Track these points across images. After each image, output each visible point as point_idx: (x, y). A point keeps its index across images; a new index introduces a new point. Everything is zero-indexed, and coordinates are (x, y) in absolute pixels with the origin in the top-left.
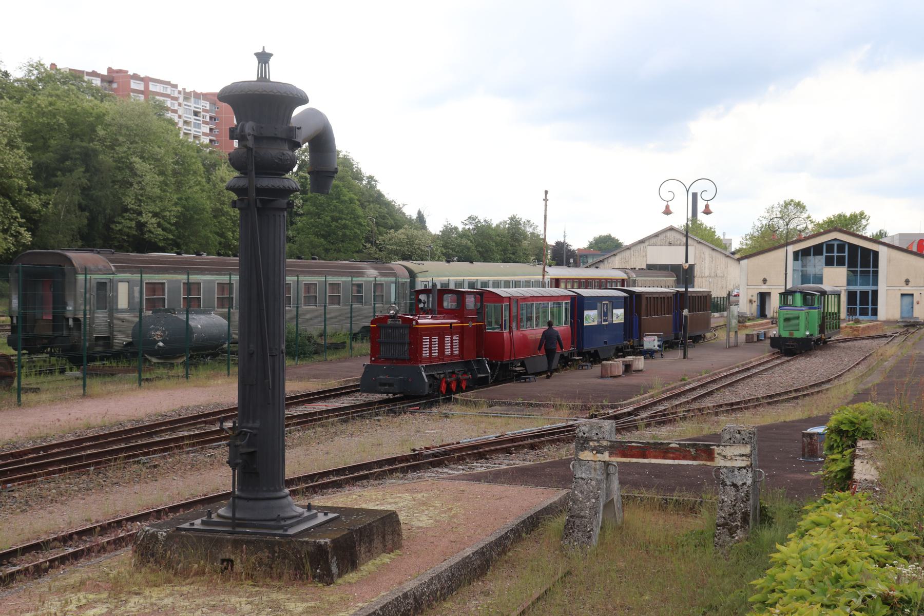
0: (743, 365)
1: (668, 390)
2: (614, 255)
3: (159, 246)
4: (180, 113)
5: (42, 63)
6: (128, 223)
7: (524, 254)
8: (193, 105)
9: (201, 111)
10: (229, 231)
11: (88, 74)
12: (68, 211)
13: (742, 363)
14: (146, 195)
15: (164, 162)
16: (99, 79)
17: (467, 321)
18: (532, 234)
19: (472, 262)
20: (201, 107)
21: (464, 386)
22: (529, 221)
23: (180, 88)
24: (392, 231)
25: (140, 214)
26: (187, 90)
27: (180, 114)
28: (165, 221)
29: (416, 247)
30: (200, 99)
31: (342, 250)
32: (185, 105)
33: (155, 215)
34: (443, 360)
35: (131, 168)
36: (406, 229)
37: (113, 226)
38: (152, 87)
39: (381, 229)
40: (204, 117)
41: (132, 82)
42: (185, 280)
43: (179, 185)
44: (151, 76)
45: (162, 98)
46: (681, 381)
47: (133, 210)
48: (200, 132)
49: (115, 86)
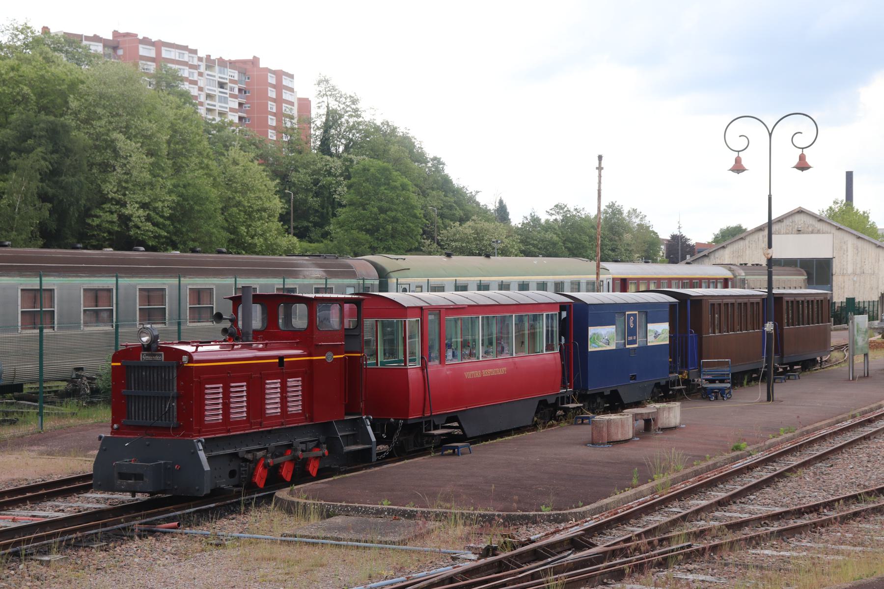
0: (864, 413)
1: (696, 473)
2: (723, 247)
4: (201, 83)
5: (29, 25)
6: (108, 217)
7: (626, 250)
8: (217, 74)
9: (227, 81)
10: (242, 225)
11: (88, 38)
12: (24, 201)
13: (860, 410)
14: (133, 181)
15: (155, 140)
16: (101, 45)
17: (323, 351)
18: (640, 226)
19: (488, 256)
20: (228, 77)
21: (313, 469)
22: (635, 210)
23: (200, 54)
24: (457, 224)
25: (124, 205)
26: (212, 58)
27: (202, 86)
28: (157, 214)
30: (227, 67)
32: (208, 75)
33: (144, 206)
34: (260, 424)
35: (111, 145)
37: (89, 221)
38: (166, 53)
39: (447, 221)
40: (232, 89)
41: (141, 46)
43: (178, 170)
44: (163, 40)
45: (175, 67)
46: (733, 450)
47: (116, 200)
48: (227, 108)
49: (120, 52)
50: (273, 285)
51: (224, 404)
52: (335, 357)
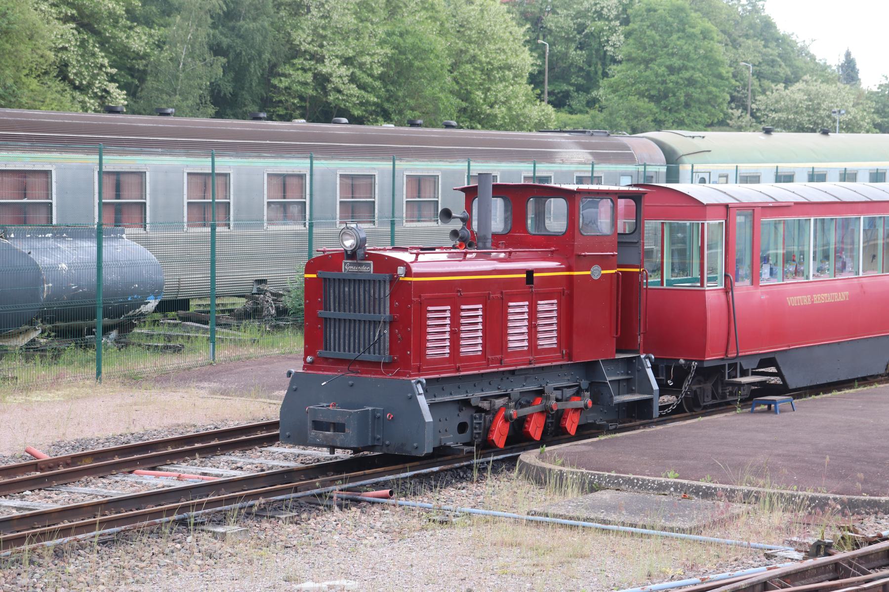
3: (353, 115)
6: (299, 76)
19: (825, 132)
21: (571, 425)
25: (321, 60)
29: (823, 113)
31: (686, 121)
33: (347, 61)
36: (806, 82)
37: (275, 81)
42: (528, 171)
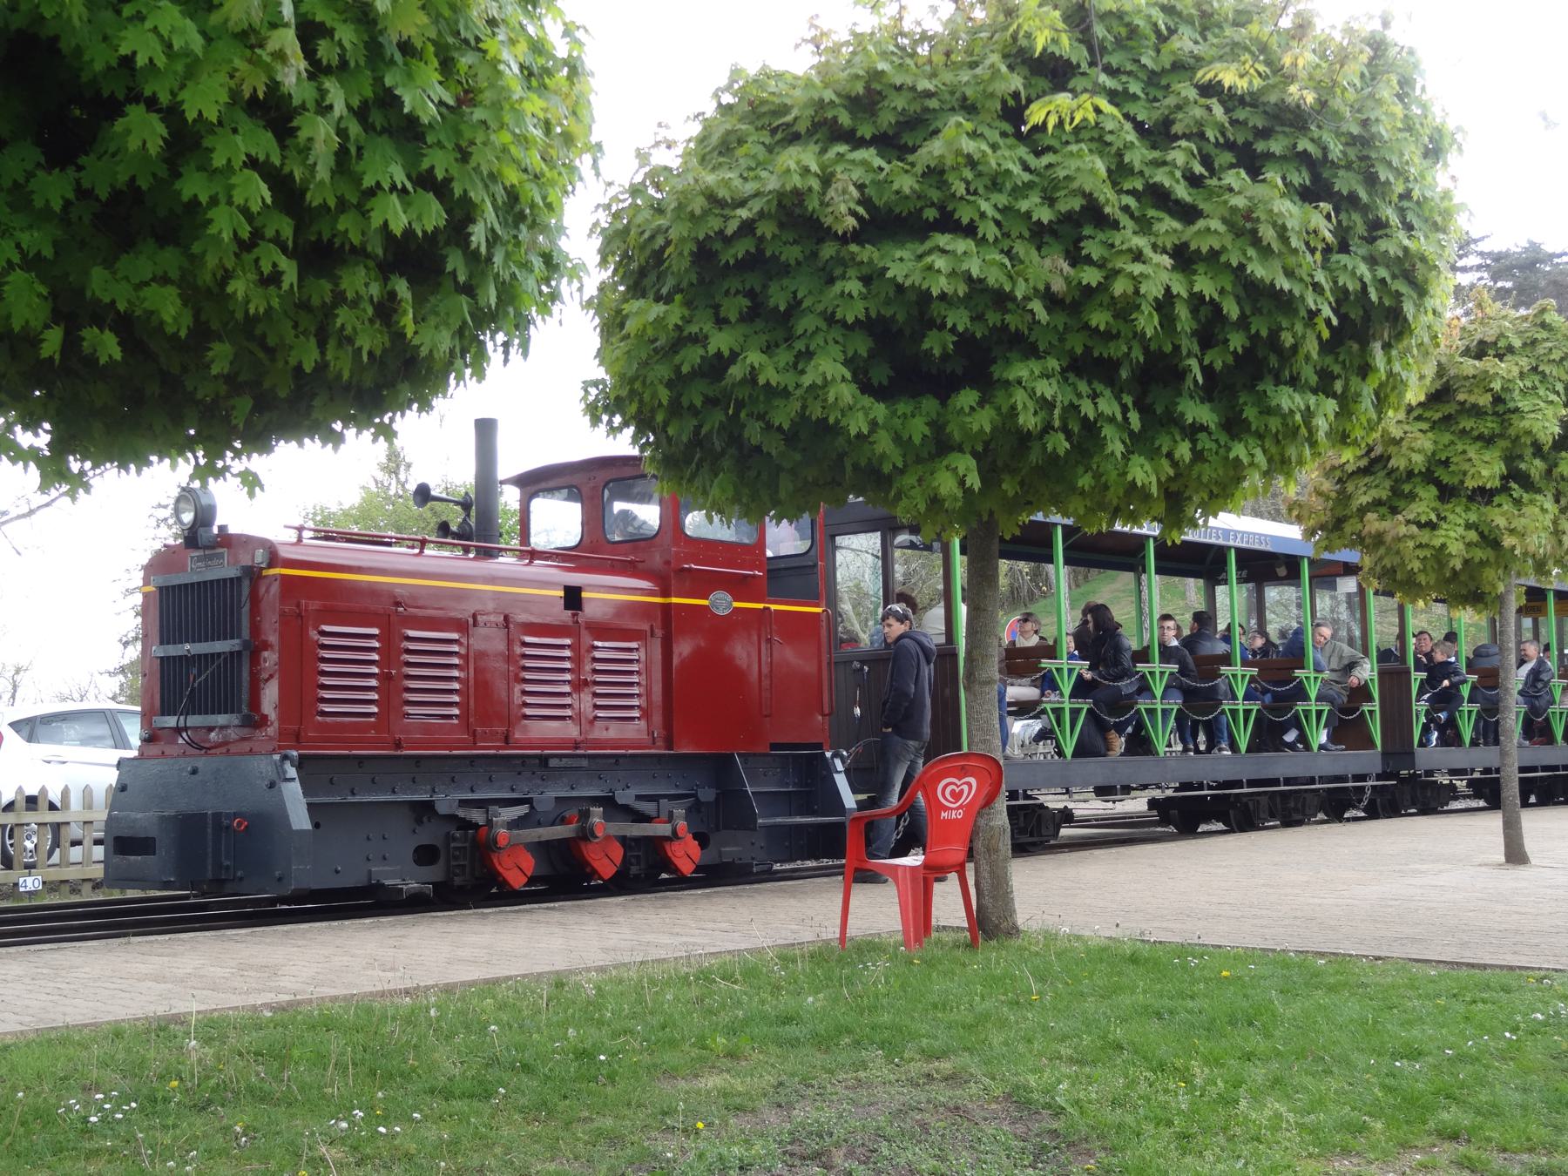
50: (962, 562)
51: (385, 678)
52: (737, 604)
